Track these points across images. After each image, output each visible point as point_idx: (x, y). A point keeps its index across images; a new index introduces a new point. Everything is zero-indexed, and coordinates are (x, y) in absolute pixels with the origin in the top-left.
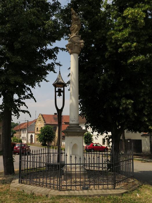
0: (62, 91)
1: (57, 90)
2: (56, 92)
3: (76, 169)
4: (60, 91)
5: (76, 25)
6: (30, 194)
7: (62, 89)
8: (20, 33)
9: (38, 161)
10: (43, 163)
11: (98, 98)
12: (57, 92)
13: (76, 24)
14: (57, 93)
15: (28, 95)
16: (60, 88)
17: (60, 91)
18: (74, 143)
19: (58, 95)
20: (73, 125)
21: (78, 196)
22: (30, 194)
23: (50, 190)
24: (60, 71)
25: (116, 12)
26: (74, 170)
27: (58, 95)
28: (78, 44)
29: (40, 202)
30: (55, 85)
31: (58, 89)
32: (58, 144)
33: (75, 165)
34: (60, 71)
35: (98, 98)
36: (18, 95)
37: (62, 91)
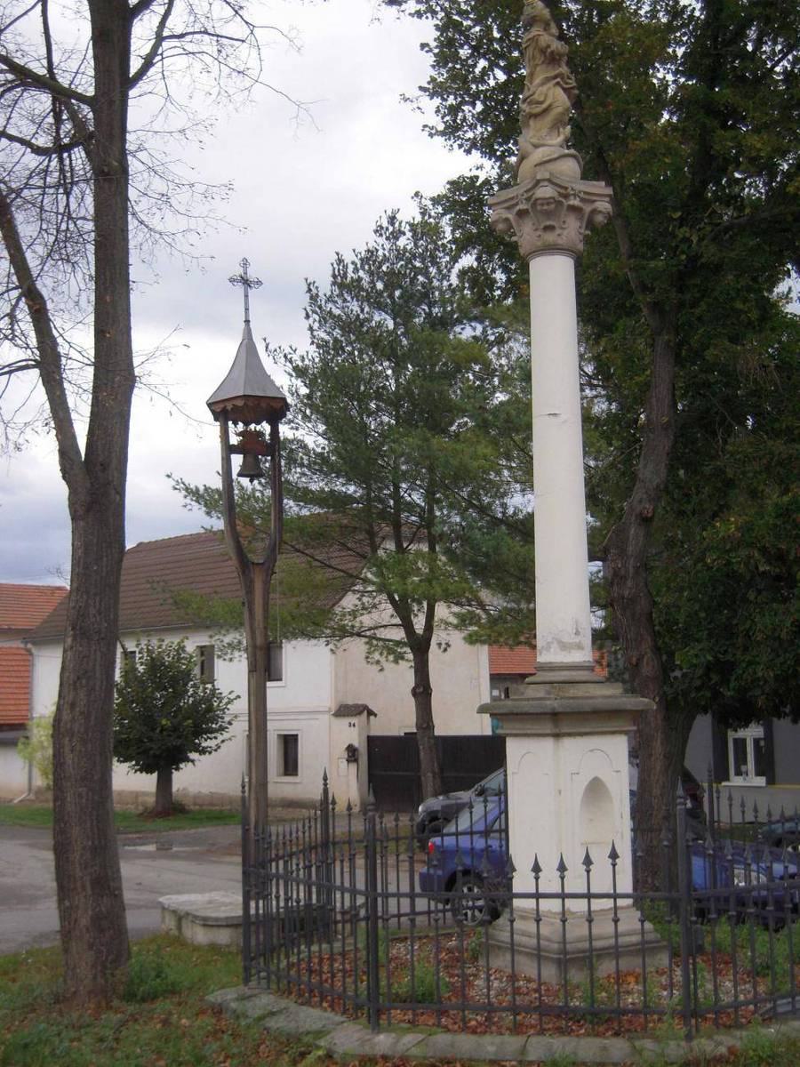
1: (234, 440)
2: (229, 449)
3: (593, 924)
5: (559, 91)
9: (347, 884)
10: (398, 895)
13: (558, 83)
14: (237, 460)
15: (751, 764)
18: (593, 777)
20: (574, 673)
23: (343, 1022)
26: (532, 927)
28: (582, 200)
29: (162, 1063)
30: (223, 410)
32: (253, 739)
33: (534, 901)
34: (247, 322)
36: (633, 754)
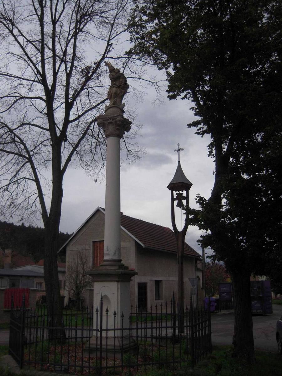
0: (184, 198)
1: (175, 196)
2: (173, 199)
4: (180, 198)
6: (147, 18)
7: (184, 193)
8: (138, 52)
11: (255, 165)
12: (175, 199)
14: (176, 202)
16: (181, 192)
17: (180, 198)
19: (177, 206)
21: (210, 323)
22: (147, 18)
24: (179, 162)
25: (254, 7)
27: (177, 206)
31: (177, 194)
34: (179, 162)
35: (255, 165)
37: (184, 198)
